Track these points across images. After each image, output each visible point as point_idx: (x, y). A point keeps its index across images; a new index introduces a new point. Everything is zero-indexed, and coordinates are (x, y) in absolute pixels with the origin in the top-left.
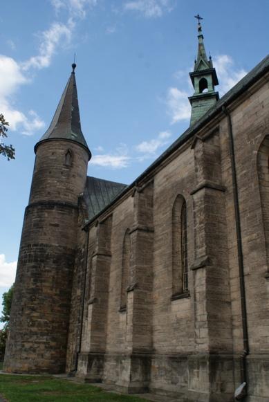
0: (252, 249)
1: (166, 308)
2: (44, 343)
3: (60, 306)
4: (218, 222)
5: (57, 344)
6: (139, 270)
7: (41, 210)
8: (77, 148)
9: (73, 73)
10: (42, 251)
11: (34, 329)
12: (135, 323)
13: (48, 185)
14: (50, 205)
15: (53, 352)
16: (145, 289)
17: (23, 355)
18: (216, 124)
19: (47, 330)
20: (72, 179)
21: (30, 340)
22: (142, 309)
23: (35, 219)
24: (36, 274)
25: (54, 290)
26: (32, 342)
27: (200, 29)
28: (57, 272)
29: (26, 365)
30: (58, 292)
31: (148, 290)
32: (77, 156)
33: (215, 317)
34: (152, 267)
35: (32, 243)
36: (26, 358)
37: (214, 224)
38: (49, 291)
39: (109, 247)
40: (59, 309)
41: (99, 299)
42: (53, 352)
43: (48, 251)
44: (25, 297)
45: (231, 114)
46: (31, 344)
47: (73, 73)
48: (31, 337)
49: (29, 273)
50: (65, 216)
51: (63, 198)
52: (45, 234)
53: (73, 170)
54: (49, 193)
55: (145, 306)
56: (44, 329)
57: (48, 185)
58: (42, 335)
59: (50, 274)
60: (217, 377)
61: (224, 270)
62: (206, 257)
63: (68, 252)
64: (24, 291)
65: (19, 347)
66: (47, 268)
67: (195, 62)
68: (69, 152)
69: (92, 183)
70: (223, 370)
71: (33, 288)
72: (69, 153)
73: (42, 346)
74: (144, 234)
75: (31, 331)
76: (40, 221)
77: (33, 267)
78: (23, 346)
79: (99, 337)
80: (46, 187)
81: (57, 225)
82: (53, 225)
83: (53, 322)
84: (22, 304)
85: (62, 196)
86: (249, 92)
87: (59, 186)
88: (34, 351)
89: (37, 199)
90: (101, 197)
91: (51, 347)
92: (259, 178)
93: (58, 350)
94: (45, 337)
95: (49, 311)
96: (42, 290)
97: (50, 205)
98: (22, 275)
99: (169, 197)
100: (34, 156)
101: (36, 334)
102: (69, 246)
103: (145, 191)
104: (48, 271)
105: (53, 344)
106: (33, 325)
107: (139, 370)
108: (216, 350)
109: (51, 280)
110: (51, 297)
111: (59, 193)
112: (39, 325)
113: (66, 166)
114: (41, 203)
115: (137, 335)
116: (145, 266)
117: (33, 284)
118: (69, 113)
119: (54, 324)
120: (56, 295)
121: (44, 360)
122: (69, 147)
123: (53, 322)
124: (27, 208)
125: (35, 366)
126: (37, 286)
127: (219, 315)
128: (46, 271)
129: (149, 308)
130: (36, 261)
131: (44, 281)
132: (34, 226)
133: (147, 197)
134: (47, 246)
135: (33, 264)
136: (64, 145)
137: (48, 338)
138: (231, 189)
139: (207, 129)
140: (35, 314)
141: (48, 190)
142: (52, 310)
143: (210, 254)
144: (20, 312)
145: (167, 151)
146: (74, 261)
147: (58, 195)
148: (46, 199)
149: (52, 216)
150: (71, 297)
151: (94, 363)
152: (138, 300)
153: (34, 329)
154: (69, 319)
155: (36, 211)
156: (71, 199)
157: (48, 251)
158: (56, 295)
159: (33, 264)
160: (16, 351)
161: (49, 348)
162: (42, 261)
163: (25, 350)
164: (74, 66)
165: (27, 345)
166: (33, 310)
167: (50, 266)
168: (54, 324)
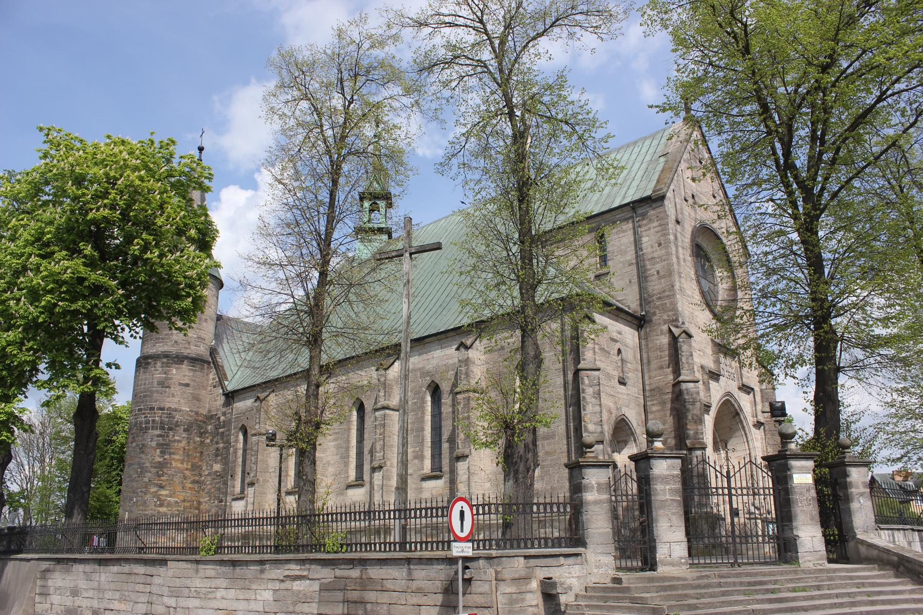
120: (187, 469)
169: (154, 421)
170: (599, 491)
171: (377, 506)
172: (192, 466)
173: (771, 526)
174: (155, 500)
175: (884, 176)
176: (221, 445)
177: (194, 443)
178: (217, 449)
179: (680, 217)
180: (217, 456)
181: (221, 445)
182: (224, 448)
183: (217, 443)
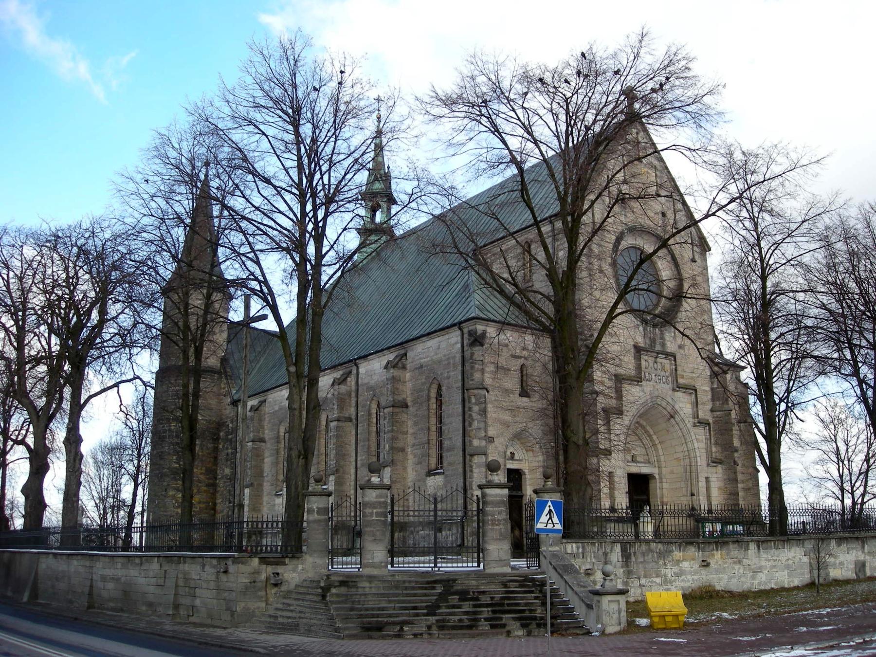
39: (264, 434)
120: (201, 474)
169: (170, 430)
170: (318, 513)
171: (265, 517)
172: (207, 470)
173: (470, 544)
174: (174, 502)
175: (744, 319)
176: (230, 451)
177: (208, 449)
178: (227, 454)
179: (695, 492)
180: (227, 460)
181: (230, 451)
182: (232, 453)
183: (227, 448)
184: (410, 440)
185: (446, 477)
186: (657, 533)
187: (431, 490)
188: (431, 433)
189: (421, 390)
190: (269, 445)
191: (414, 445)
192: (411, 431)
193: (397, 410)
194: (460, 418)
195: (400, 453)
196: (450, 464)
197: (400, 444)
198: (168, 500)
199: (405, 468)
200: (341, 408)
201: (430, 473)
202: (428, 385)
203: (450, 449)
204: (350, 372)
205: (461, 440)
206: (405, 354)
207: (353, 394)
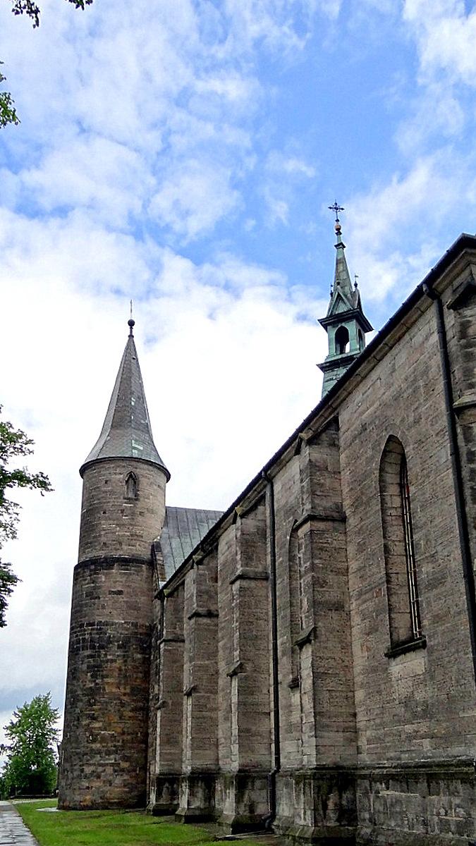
0: (284, 655)
1: (378, 671)
2: (112, 765)
3: (132, 710)
4: (257, 619)
5: (131, 765)
6: (197, 669)
7: (95, 572)
8: (142, 470)
9: (131, 336)
10: (100, 631)
11: (97, 746)
12: (194, 736)
13: (103, 533)
14: (108, 563)
15: (126, 777)
16: (207, 692)
17: (83, 783)
18: (261, 491)
19: (115, 746)
20: (140, 518)
21: (91, 762)
22: (204, 718)
23: (87, 586)
24: (95, 666)
25: (121, 688)
26: (94, 764)
27: (339, 233)
28: (125, 661)
29: (88, 797)
30: (128, 691)
31: (212, 693)
32: (143, 482)
33: (248, 731)
34: (216, 663)
35: (85, 621)
36: (88, 788)
37: (252, 622)
38: (114, 690)
39: (182, 629)
40: (131, 714)
41: (170, 702)
42: (126, 777)
43: (110, 631)
44: (82, 701)
45: (273, 481)
46: (92, 768)
47: (131, 336)
48: (92, 757)
49: (84, 667)
50: (131, 577)
51: (125, 552)
52: (103, 607)
53: (139, 504)
54: (105, 544)
55: (208, 714)
56: (109, 745)
57: (103, 533)
58: (109, 753)
59: (114, 665)
60: (246, 797)
61: (263, 676)
62: (239, 663)
63: (141, 631)
64: (79, 692)
65: (76, 773)
66: (109, 657)
67: (332, 294)
68: (131, 476)
69: (174, 517)
70: (253, 789)
71: (91, 688)
72: (133, 479)
73: (109, 770)
74: (205, 620)
75: (92, 750)
76: (94, 588)
77: (90, 656)
78: (82, 771)
79: (170, 753)
80: (100, 536)
81: (120, 593)
82: (114, 593)
83: (123, 733)
84: (78, 710)
85: (125, 547)
86: (283, 459)
87: (120, 532)
88: (99, 777)
89: (91, 554)
90: (188, 540)
91: (123, 770)
92: (290, 571)
93: (133, 774)
94: (112, 756)
95: (116, 719)
96: (104, 689)
97: (108, 563)
98: (75, 669)
99: (230, 572)
100: (79, 482)
101: (99, 753)
102: (141, 621)
103: (205, 562)
104: (112, 661)
105: (125, 765)
106: (94, 741)
107: (200, 794)
108: (247, 768)
109: (116, 674)
110: (119, 699)
111: (120, 544)
112: (103, 740)
113: (129, 499)
114: (94, 561)
115: (196, 751)
116: (206, 662)
117: (91, 682)
118: (128, 407)
119: (125, 737)
120: (125, 694)
121: (112, 788)
122: (131, 469)
123: (123, 733)
124: (76, 568)
125: (101, 798)
126: (97, 684)
127: (254, 728)
128: (107, 661)
129: (212, 715)
130: (93, 647)
131: (107, 676)
132: (87, 596)
133: (209, 569)
134: (107, 624)
135: (88, 652)
136: (121, 470)
137: (118, 757)
138: (271, 577)
139: (256, 492)
140: (97, 725)
141: (103, 539)
142: (120, 718)
143: (244, 659)
144: (75, 723)
145: (250, 485)
146: (151, 642)
147: (118, 547)
148: (102, 554)
149: (112, 579)
150: (149, 695)
151: (165, 789)
152: (198, 707)
153: (97, 746)
154: (148, 728)
155: (88, 573)
156: (143, 551)
157: (110, 631)
158: (125, 694)
159: (88, 652)
160: (73, 779)
161: (119, 771)
162: (102, 647)
163: (86, 777)
164: (131, 324)
165: (88, 770)
166: (94, 718)
167: (114, 653)
168: (125, 737)
172: (132, 689)
177: (134, 661)
184: (354, 583)
185: (430, 653)
186: (137, 734)
187: (401, 690)
188: (393, 559)
189: (366, 475)
190: (187, 645)
191: (360, 594)
192: (353, 566)
193: (321, 525)
194: (453, 499)
195: (334, 614)
196: (437, 619)
197: (332, 595)
198: (80, 731)
199: (346, 647)
200: (248, 558)
201: (398, 649)
202: (378, 459)
203: (437, 581)
204: (263, 497)
205: (457, 554)
206: (336, 420)
207: (268, 531)
